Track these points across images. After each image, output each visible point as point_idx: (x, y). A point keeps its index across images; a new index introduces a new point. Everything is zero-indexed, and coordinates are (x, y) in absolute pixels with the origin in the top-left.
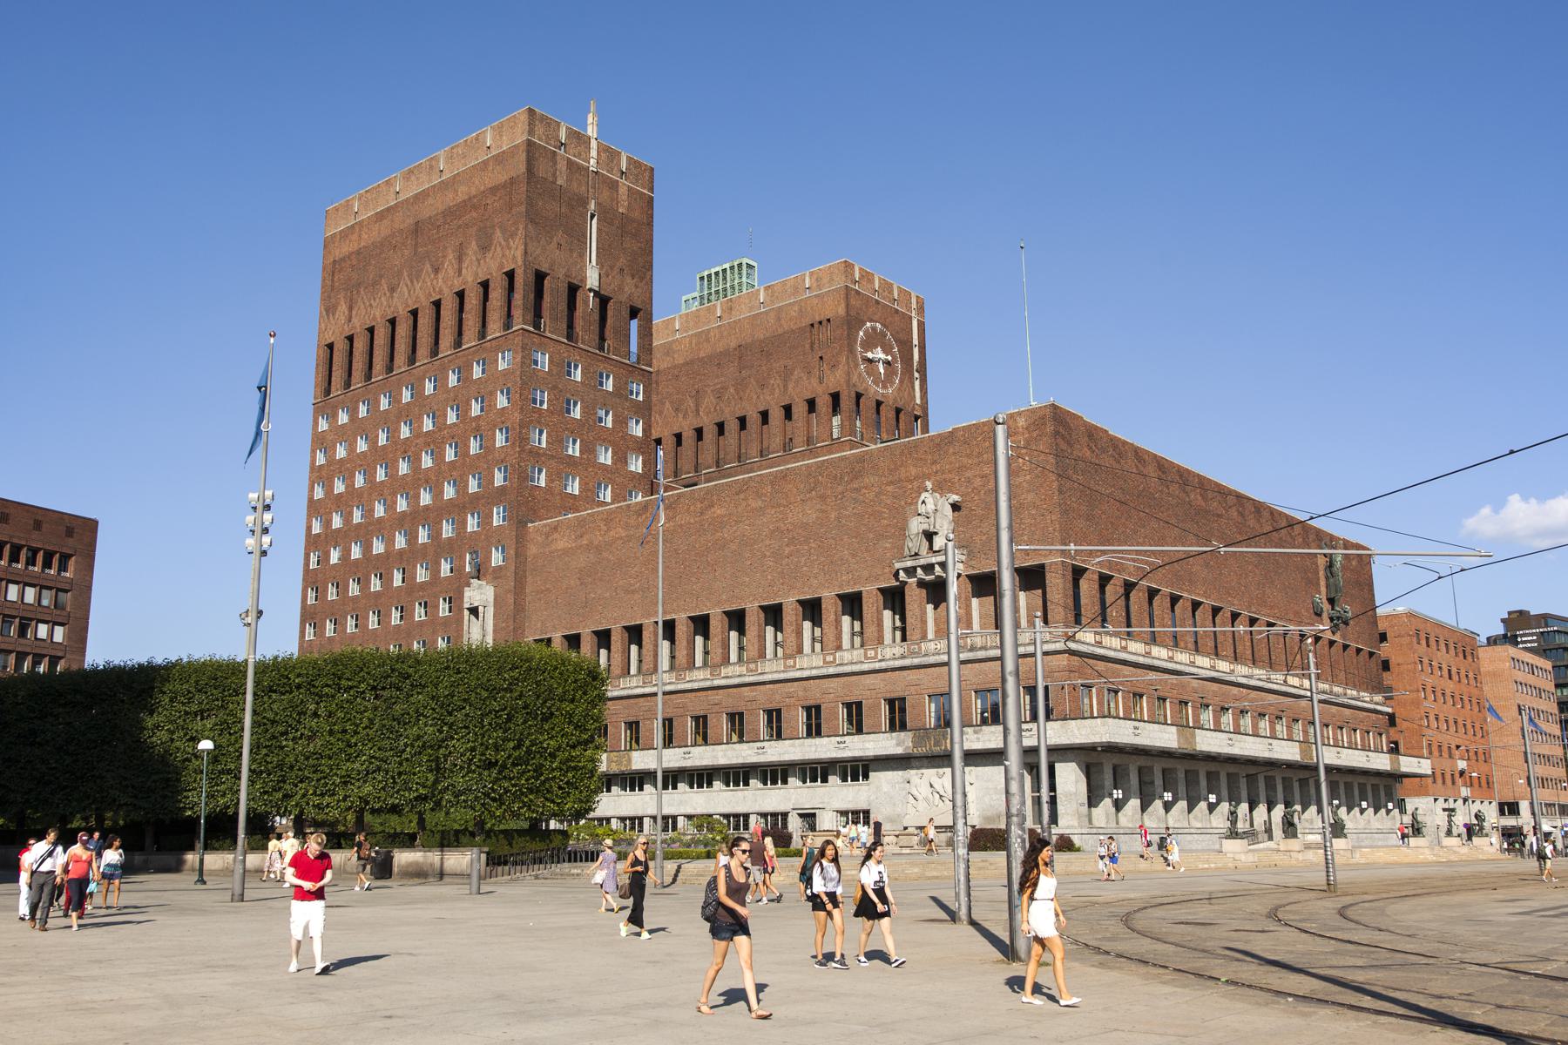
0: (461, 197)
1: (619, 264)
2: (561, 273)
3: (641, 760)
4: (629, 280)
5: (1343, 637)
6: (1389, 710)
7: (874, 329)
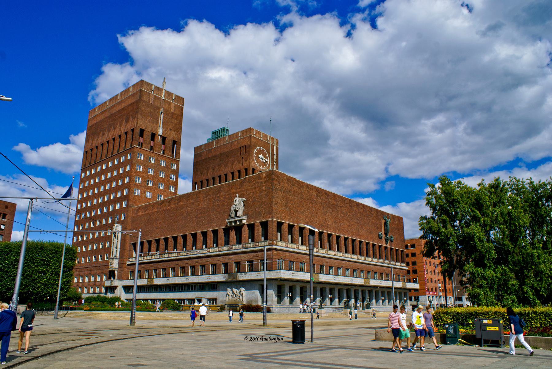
0: (123, 107)
1: (170, 127)
2: (150, 129)
3: (242, 277)
4: (173, 132)
5: (390, 245)
6: (407, 268)
7: (260, 149)
